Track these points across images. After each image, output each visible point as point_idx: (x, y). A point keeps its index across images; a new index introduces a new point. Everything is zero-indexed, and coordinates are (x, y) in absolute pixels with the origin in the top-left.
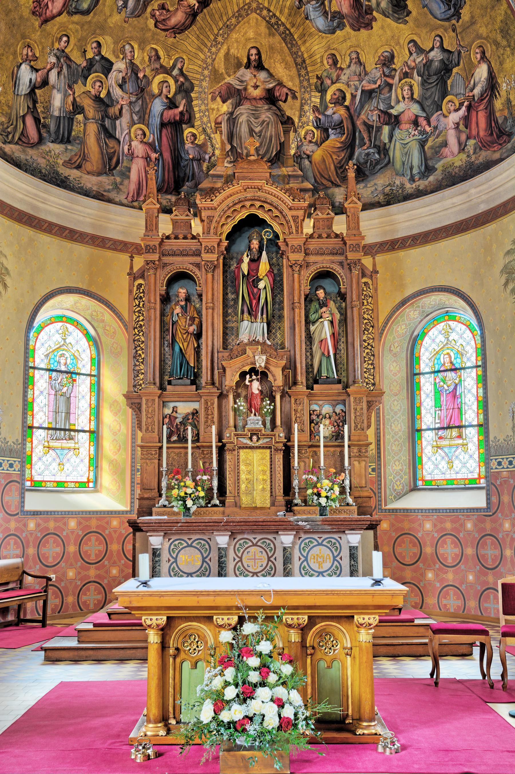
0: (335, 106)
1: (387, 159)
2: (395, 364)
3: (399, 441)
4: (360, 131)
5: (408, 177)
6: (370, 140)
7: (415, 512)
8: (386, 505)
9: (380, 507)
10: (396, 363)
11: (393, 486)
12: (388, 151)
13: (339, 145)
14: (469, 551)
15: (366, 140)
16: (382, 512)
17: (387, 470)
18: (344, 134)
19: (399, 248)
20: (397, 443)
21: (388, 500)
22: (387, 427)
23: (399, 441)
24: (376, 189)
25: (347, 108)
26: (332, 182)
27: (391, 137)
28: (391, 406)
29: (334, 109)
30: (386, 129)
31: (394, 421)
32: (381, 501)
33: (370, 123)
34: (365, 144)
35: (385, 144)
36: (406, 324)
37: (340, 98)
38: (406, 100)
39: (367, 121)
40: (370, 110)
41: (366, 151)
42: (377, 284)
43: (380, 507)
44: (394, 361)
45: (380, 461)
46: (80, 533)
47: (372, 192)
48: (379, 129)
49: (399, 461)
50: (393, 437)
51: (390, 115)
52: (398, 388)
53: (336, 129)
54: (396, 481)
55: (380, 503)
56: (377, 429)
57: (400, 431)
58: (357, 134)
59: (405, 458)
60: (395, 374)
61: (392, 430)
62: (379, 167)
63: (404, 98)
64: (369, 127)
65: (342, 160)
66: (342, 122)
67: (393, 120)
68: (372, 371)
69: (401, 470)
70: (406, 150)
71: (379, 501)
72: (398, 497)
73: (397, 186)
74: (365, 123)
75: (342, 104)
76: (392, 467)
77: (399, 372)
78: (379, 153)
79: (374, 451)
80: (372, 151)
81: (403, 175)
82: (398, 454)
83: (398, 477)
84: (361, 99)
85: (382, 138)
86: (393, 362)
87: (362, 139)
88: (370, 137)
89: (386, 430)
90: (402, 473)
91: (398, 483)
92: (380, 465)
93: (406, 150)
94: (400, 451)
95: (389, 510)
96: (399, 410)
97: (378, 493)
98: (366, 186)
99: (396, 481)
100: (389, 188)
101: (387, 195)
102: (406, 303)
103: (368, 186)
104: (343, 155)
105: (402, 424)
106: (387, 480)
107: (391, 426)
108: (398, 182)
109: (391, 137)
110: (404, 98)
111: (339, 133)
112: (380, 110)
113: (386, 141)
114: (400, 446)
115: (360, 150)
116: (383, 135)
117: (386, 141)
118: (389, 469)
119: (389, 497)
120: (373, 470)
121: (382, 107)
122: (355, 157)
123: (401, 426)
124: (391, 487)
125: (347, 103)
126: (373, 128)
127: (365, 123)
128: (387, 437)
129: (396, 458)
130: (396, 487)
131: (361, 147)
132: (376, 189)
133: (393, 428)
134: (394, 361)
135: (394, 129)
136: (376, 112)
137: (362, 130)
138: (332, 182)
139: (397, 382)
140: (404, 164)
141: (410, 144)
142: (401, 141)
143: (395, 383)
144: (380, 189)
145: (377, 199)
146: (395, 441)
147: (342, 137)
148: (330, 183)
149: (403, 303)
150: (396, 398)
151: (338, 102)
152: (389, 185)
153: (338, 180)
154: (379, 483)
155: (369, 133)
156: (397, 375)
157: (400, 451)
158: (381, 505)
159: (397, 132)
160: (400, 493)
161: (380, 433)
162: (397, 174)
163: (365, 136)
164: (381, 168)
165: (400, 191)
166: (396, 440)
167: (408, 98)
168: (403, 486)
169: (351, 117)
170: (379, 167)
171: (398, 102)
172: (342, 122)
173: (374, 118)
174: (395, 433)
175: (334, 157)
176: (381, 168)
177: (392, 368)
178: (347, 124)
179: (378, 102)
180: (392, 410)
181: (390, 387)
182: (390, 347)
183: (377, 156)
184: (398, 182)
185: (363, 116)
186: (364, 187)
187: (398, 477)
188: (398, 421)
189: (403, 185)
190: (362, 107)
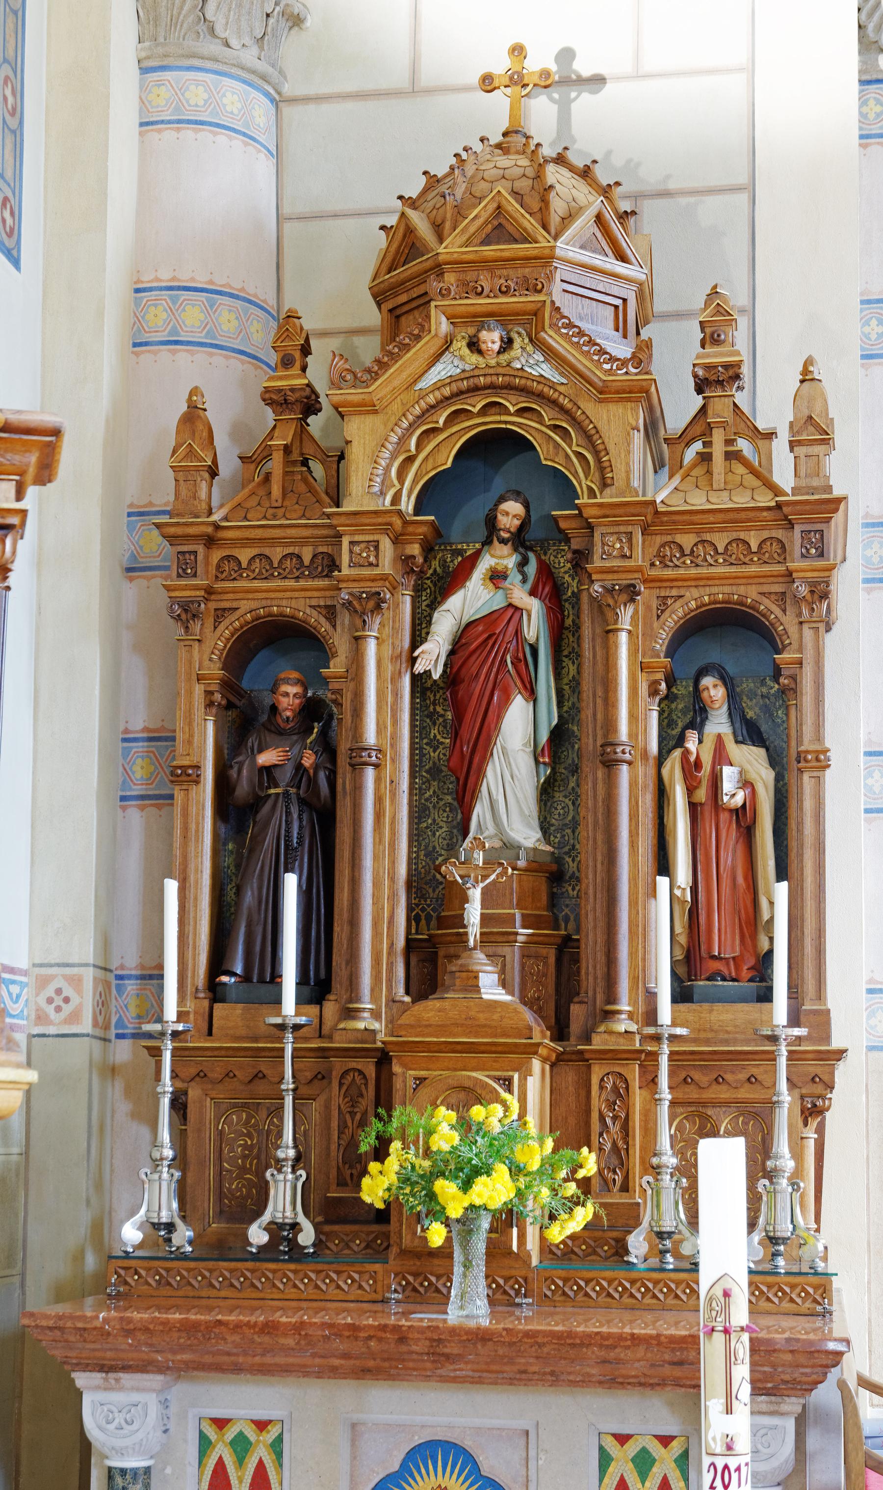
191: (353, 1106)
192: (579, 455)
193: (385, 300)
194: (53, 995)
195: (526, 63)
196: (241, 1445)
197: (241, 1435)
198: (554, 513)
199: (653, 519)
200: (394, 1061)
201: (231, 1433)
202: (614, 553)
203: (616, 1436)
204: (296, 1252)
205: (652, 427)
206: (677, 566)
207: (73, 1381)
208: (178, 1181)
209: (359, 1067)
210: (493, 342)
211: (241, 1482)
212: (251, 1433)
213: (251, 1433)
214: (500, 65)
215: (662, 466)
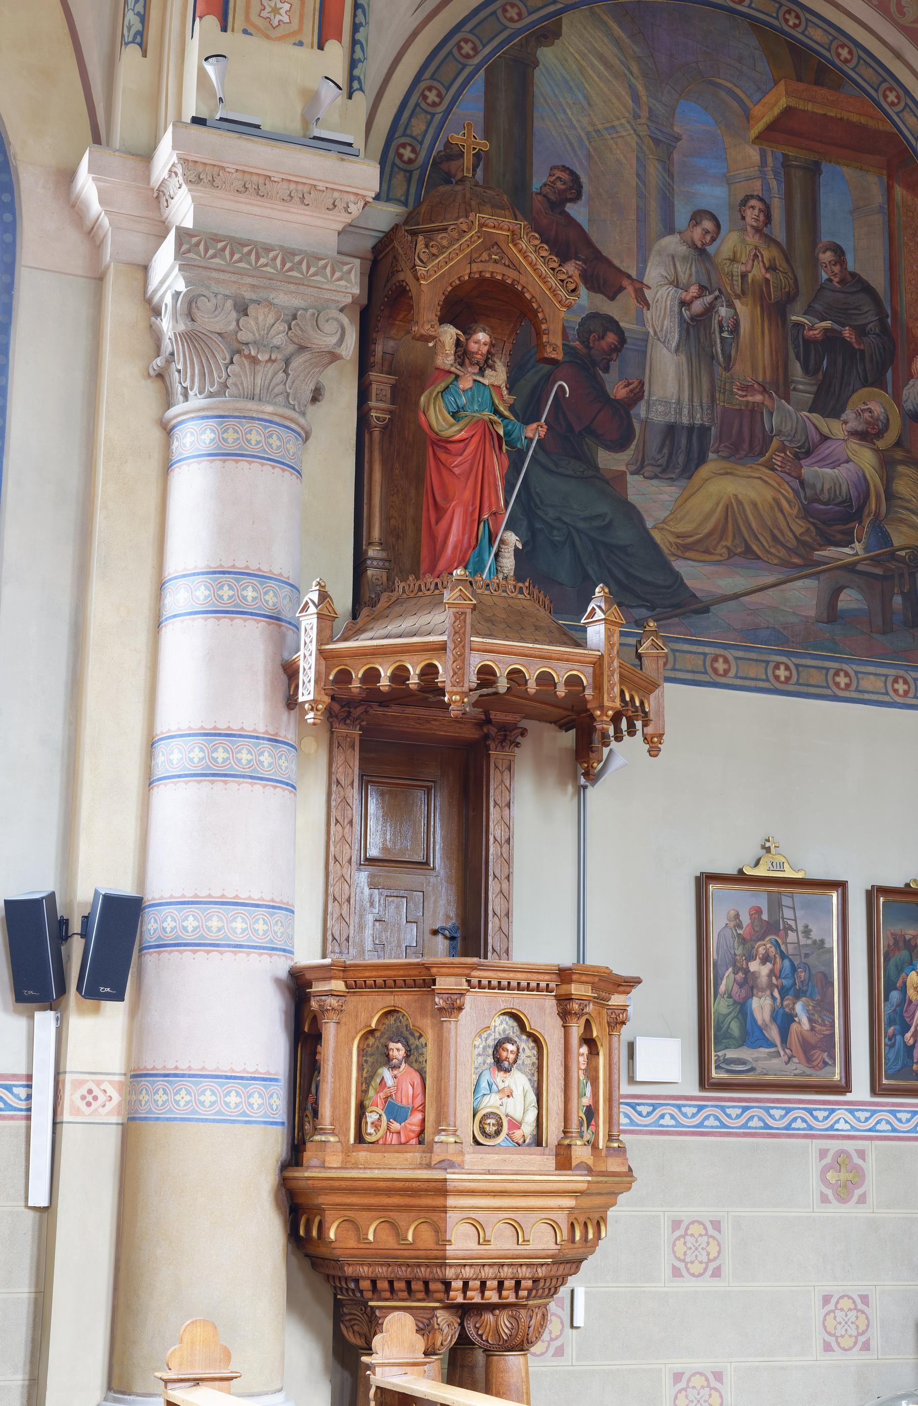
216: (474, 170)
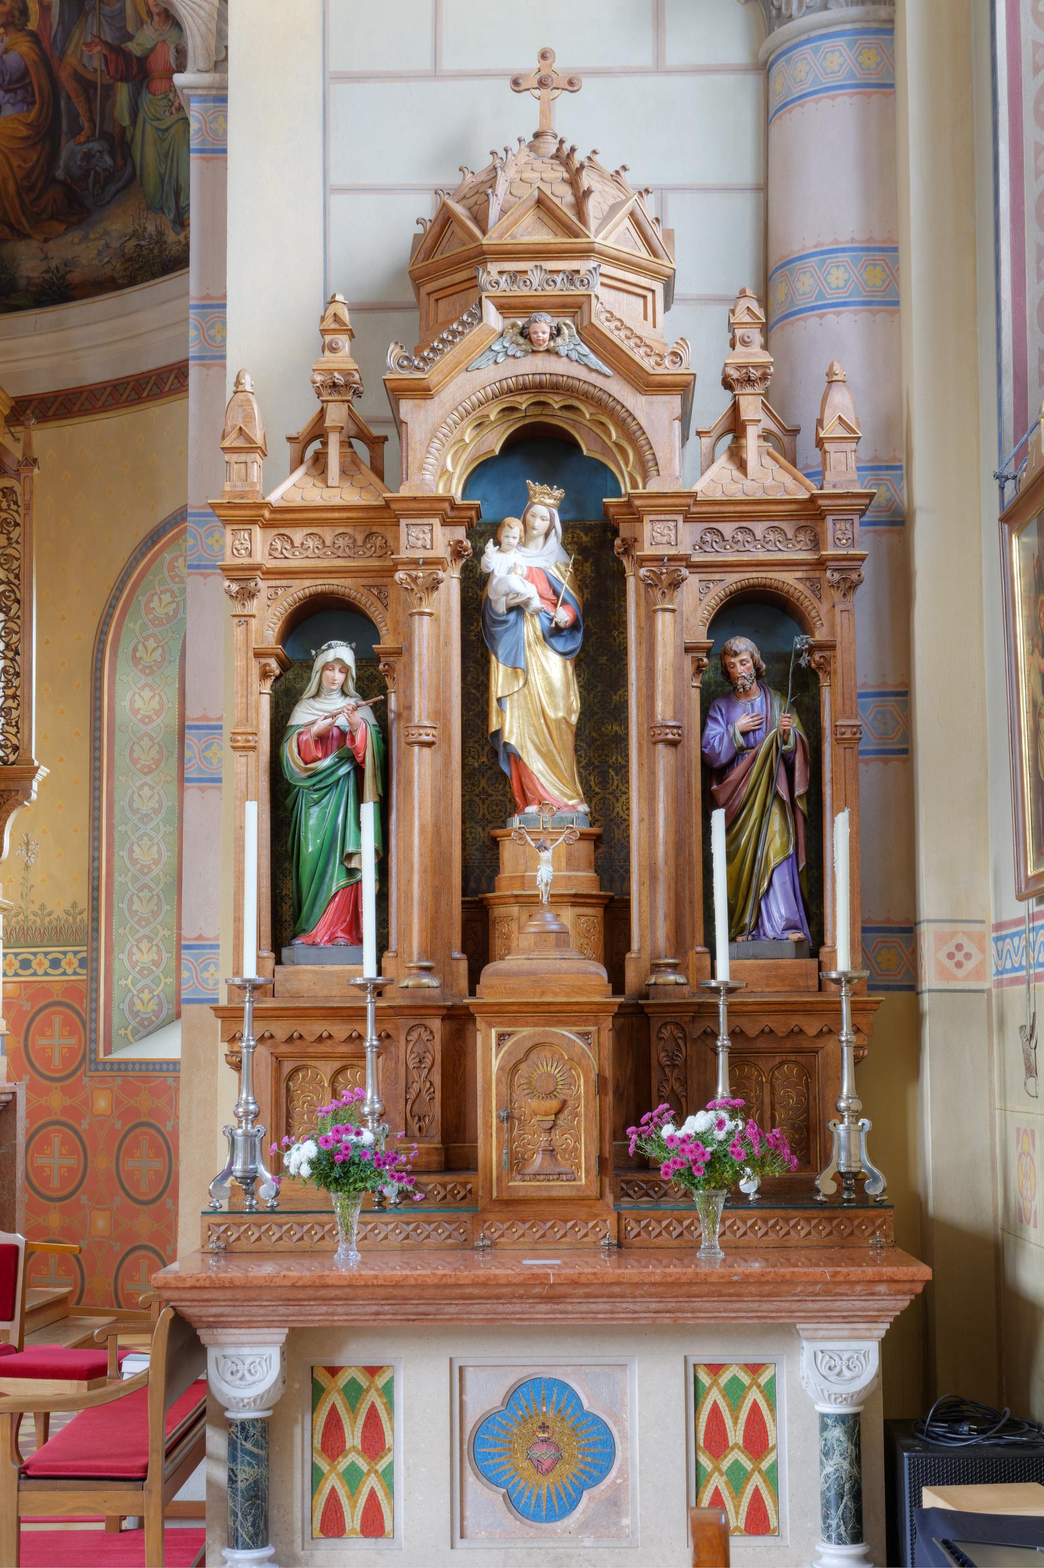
0: (6, 33)
1: (129, 169)
2: (147, 693)
3: (151, 890)
4: (69, 98)
5: (172, 216)
6: (92, 120)
7: (161, 1070)
8: (108, 1051)
9: (93, 1056)
10: (152, 689)
11: (132, 1004)
12: (129, 148)
13: (25, 132)
14: (102, 1163)
15: (84, 120)
16: (97, 1070)
17: (116, 965)
18: (34, 103)
19: (152, 397)
20: (145, 893)
21: (115, 1039)
22: (121, 854)
23: (151, 890)
24: (107, 246)
25: (35, 38)
26: (12, 228)
27: (134, 112)
28: (132, 800)
29: (6, 39)
30: (123, 93)
31: (141, 838)
32: (96, 1041)
33: (89, 76)
34: (82, 129)
35: (124, 129)
36: (172, 592)
37: (16, 13)
38: (156, 18)
39: (80, 69)
40: (86, 44)
41: (85, 148)
42: (32, 493)
43: (93, 1056)
44: (146, 685)
45: (97, 939)
46: (118, 1125)
47: (99, 253)
48: (109, 92)
49: (150, 940)
50: (135, 879)
51: (127, 55)
52: (154, 753)
53: (14, 91)
54: (141, 991)
55: (93, 1046)
56: (94, 859)
57: (156, 862)
58: (63, 103)
59: (167, 933)
60: (147, 720)
61: (134, 862)
62: (113, 188)
63: (150, 14)
64: (86, 86)
65: (32, 169)
66: (25, 73)
67: (135, 69)
68: (15, 713)
69: (156, 964)
70: (166, 145)
71: (91, 1041)
72: (143, 1032)
73: (151, 235)
74: (78, 78)
75: (21, 29)
76: (131, 954)
77: (158, 713)
78: (112, 154)
79: (85, 916)
80: (96, 146)
81: (161, 209)
82: (149, 923)
83: (147, 981)
84: (61, 14)
85: (117, 113)
86: (142, 689)
87: (74, 117)
88: (91, 111)
89: (117, 863)
90: (158, 971)
91: (146, 996)
92: (97, 950)
93: (166, 145)
94: (155, 914)
95: (112, 1063)
96: (156, 811)
97: (91, 1020)
98: (85, 238)
99: (141, 991)
100: (133, 242)
101: (130, 259)
102: (160, 538)
103: (92, 236)
104: (35, 158)
105: (163, 847)
106: (116, 987)
107: (131, 851)
108: (151, 228)
109: (134, 112)
110: (150, 14)
111: (23, 101)
112: (106, 43)
113: (126, 122)
114: (155, 900)
115: (71, 143)
116: (118, 104)
117: (126, 122)
118: (121, 959)
119: (118, 1031)
120: (83, 963)
121: (108, 36)
122: (62, 163)
123: (159, 852)
124: (125, 1007)
125: (32, 25)
126: (96, 89)
127: (78, 78)
128: (119, 879)
129: (142, 932)
130: (138, 1005)
131: (74, 136)
132: (107, 246)
133: (135, 856)
134: (146, 685)
135: (139, 93)
136: (99, 48)
137: (72, 94)
138: (12, 228)
139: (151, 738)
140: (162, 181)
141: (172, 130)
142: (156, 123)
143: (146, 742)
144: (115, 244)
145: (108, 270)
146: (140, 889)
147: (29, 111)
148: (7, 230)
149: (154, 537)
150: (148, 779)
151: (13, 23)
152: (134, 234)
153: (24, 220)
154: (94, 995)
155: (89, 101)
156: (151, 721)
157: (155, 914)
158: (96, 1051)
159: (146, 98)
160: (151, 1022)
161: (99, 869)
162: (149, 208)
163: (81, 108)
164: (118, 191)
165: (156, 251)
166: (146, 886)
167: (159, 14)
168: (160, 1004)
169: (45, 60)
170: (113, 188)
171: (141, 23)
172: (25, 73)
173: (95, 60)
174: (141, 870)
175: (15, 162)
176: (118, 191)
177: (139, 704)
178: (36, 77)
179: (100, 22)
180: (135, 812)
181: (132, 751)
182: (135, 650)
183: (108, 160)
184: (151, 228)
185: (71, 59)
186: (81, 241)
187: (147, 981)
188: (151, 839)
189: (161, 234)
190: (67, 35)
191: (420, 1061)
192: (616, 444)
193: (423, 284)
194: (965, 950)
195: (555, 66)
196: (735, 1392)
197: (735, 1379)
198: (605, 500)
199: (689, 508)
200: (478, 1019)
201: (724, 1378)
202: (657, 537)
203: (709, 1366)
204: (864, 1201)
205: (685, 418)
206: (286, 558)
207: (198, 1337)
208: (869, 1135)
209: (678, 1020)
210: (544, 333)
211: (735, 1423)
212: (363, 1381)
213: (363, 1381)
214: (529, 64)
215: (302, 462)
216: (485, 532)
